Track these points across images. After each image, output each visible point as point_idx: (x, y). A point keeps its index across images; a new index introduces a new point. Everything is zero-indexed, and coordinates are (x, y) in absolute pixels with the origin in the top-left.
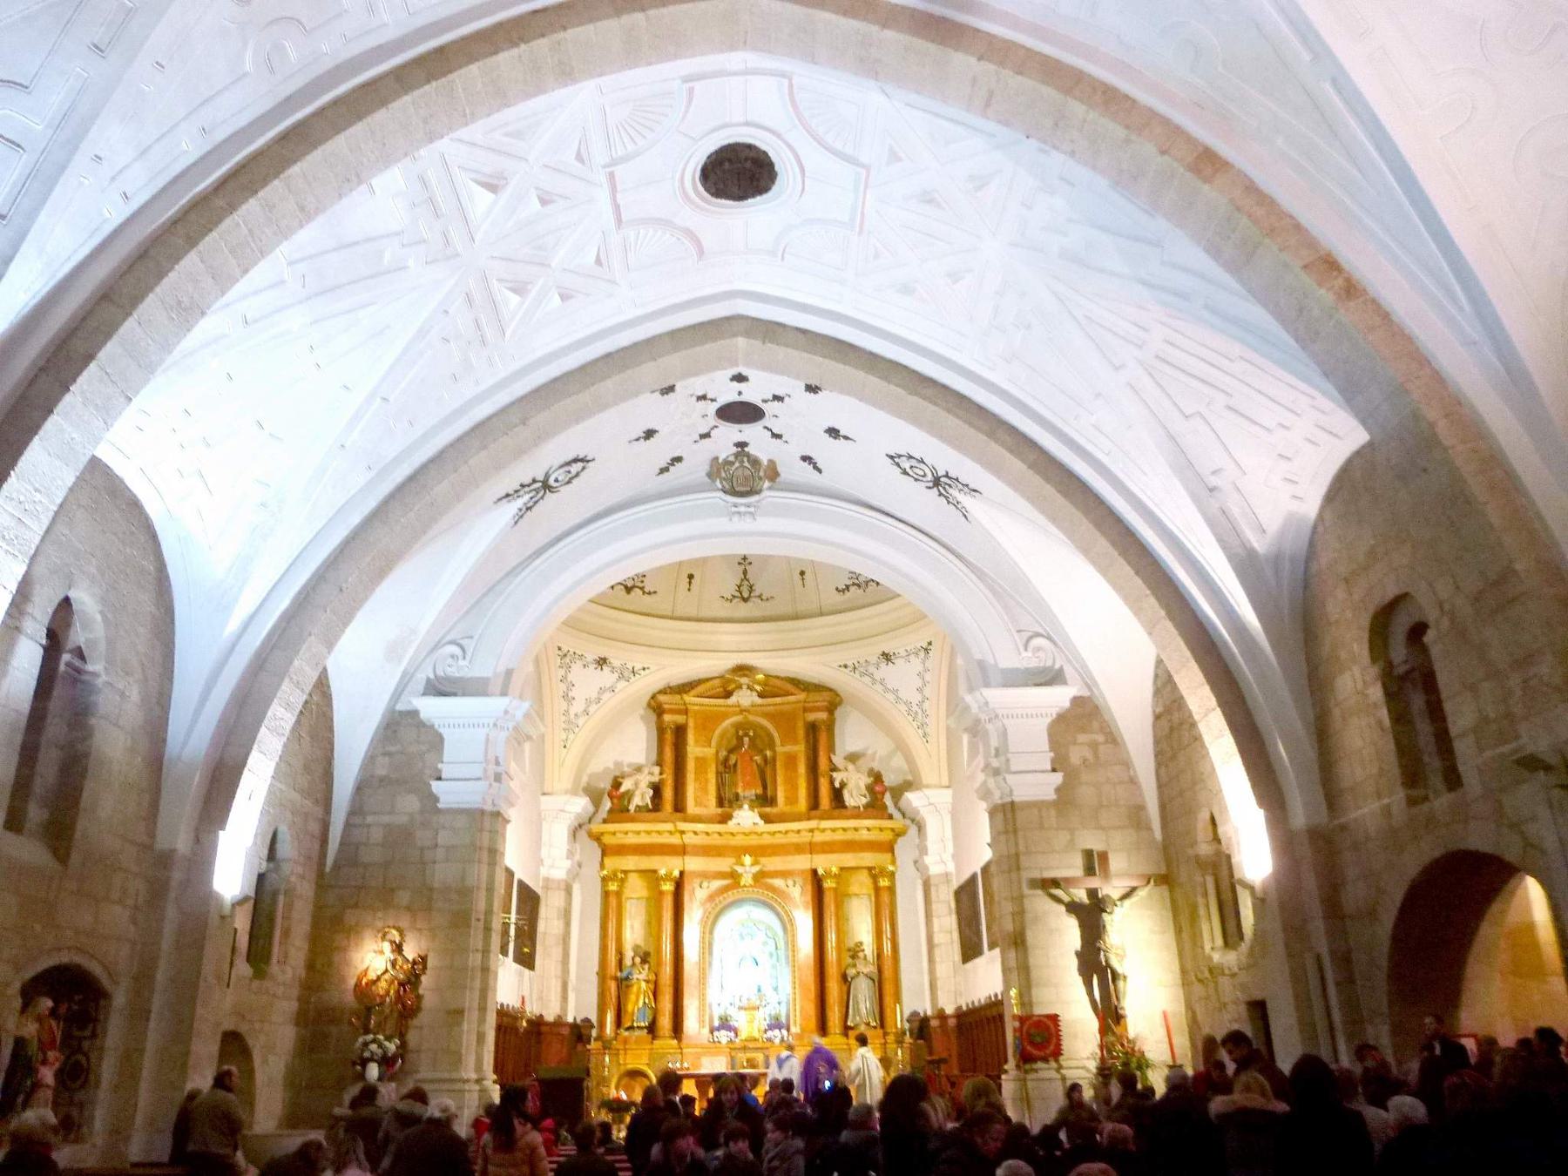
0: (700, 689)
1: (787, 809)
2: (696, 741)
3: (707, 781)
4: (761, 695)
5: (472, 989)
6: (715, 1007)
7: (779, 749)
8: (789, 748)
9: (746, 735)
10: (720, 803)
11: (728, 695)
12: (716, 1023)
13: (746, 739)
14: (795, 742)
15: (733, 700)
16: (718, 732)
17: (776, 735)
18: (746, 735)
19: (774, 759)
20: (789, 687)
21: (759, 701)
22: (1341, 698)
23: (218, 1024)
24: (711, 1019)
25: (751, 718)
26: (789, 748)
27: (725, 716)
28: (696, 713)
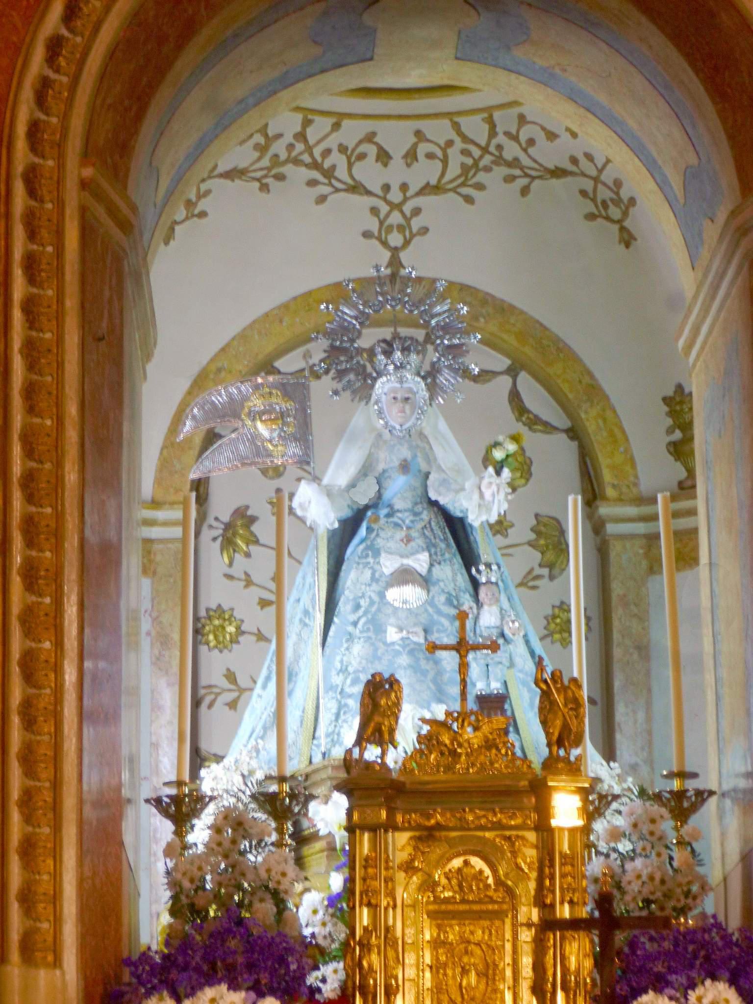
6: (149, 839)
12: (152, 922)
24: (106, 900)
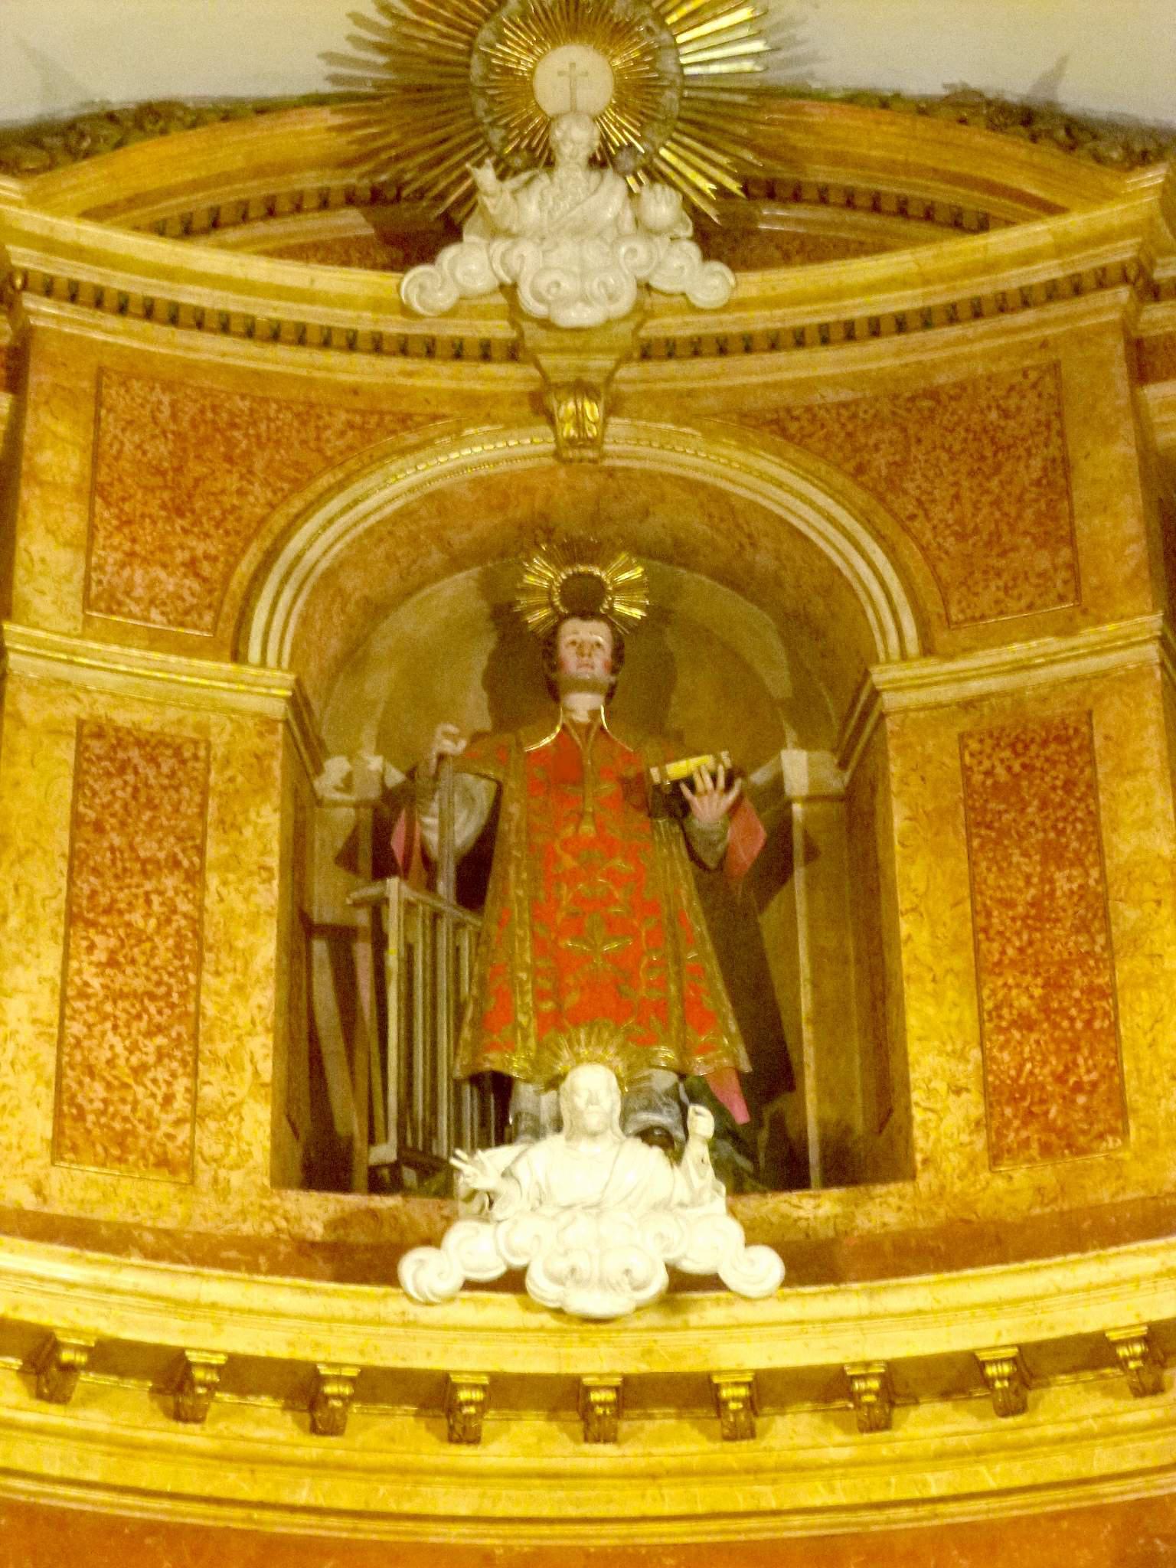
0: (148, 163)
1: (1016, 1188)
2: (99, 601)
3: (194, 945)
4: (719, 238)
5: (985, 247)
7: (909, 682)
8: (1018, 664)
9: (585, 601)
10: (322, 1163)
11: (415, 229)
13: (585, 644)
14: (1074, 599)
15: (465, 268)
16: (319, 539)
17: (870, 570)
18: (585, 601)
19: (857, 809)
20: (1014, 163)
21: (709, 284)
22: (831, 1234)
23: (263, 1188)
25: (627, 443)
26: (1018, 664)
27: (387, 426)
28: (107, 376)
